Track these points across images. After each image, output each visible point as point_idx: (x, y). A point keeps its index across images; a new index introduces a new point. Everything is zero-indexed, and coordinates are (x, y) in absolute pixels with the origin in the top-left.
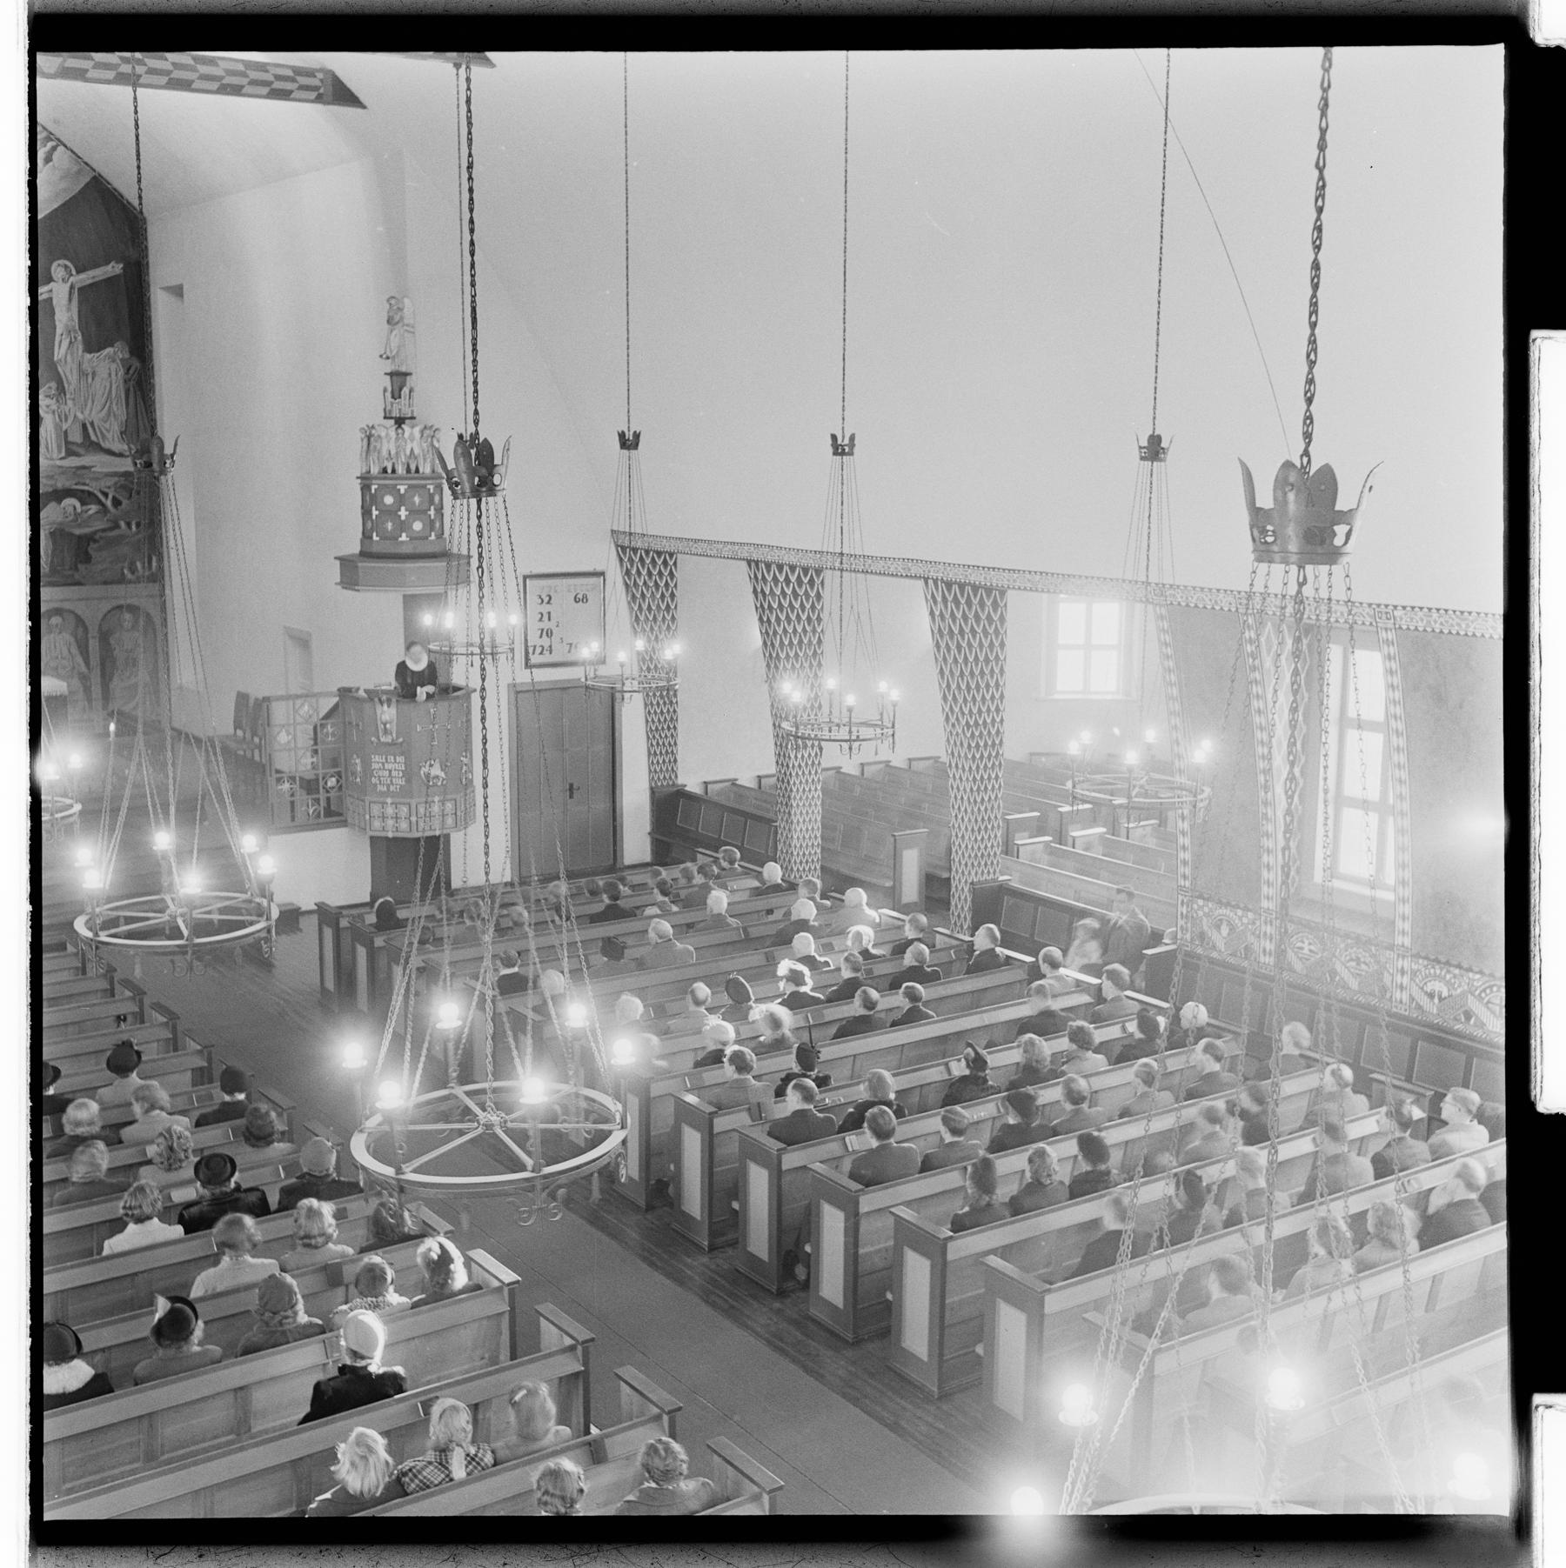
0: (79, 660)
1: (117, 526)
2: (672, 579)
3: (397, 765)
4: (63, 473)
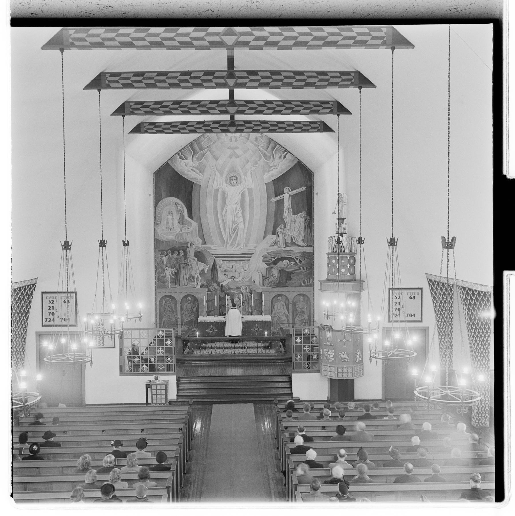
0: (286, 311)
1: (300, 269)
3: (331, 353)
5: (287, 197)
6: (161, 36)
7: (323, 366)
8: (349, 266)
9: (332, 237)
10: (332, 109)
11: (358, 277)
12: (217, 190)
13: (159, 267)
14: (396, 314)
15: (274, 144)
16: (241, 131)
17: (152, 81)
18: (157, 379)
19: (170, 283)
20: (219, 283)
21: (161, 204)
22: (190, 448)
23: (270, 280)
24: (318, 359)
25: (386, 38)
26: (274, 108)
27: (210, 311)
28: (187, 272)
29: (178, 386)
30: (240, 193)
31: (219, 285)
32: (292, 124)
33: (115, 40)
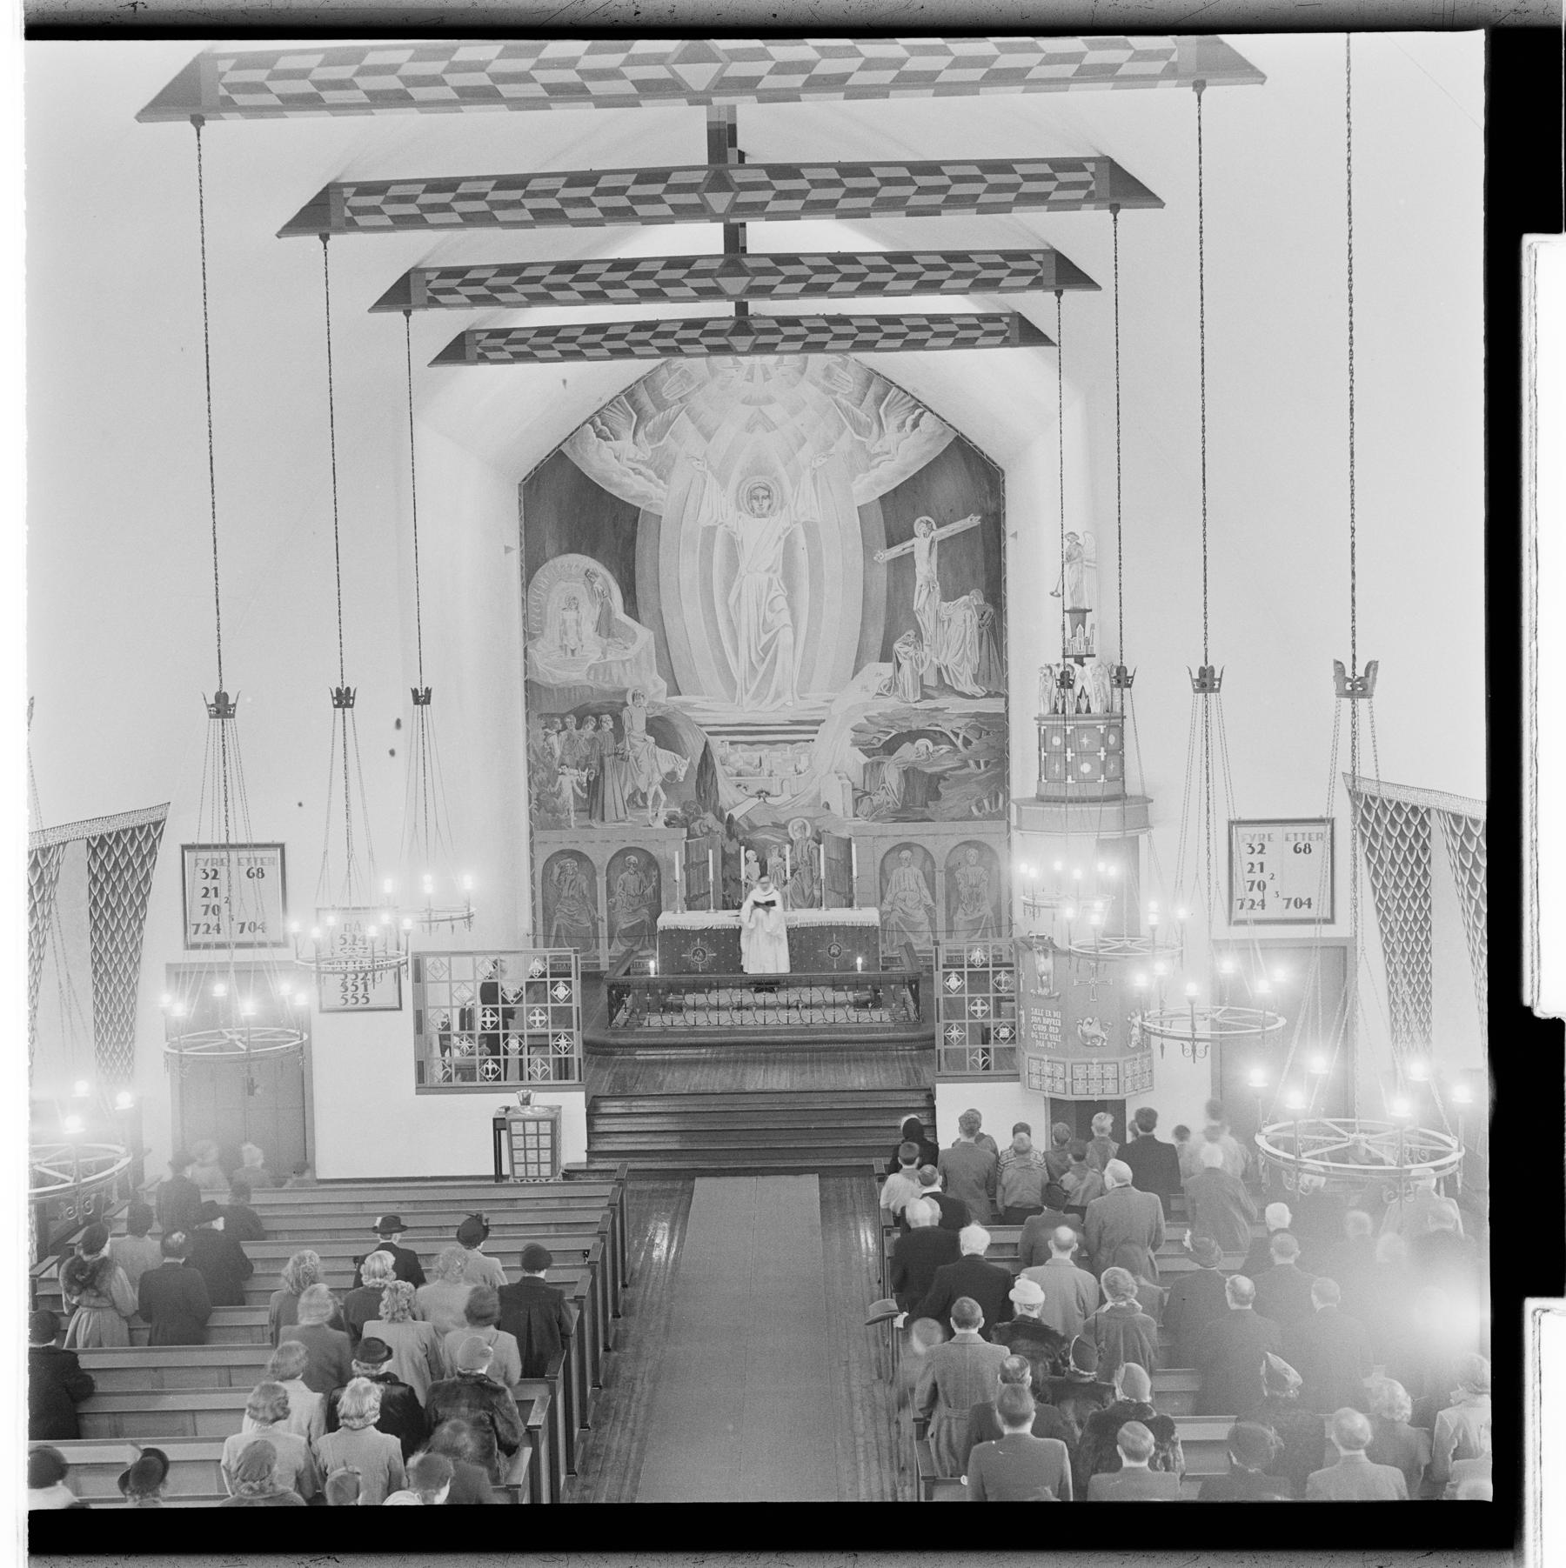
0: (926, 892)
2: (1424, 829)
4: (918, 715)
5: (923, 545)
6: (491, 69)
7: (1027, 1059)
8: (1102, 754)
9: (1049, 667)
10: (1040, 274)
11: (1132, 788)
12: (710, 531)
13: (540, 769)
14: (1253, 901)
15: (882, 387)
16: (769, 348)
17: (481, 206)
18: (526, 1101)
19: (572, 814)
20: (721, 810)
21: (542, 576)
22: (620, 1310)
23: (876, 799)
24: (1014, 1038)
25: (1176, 53)
26: (861, 276)
27: (697, 897)
28: (626, 780)
29: (590, 1124)
30: (780, 538)
31: (720, 817)
32: (925, 322)
33: (355, 87)
